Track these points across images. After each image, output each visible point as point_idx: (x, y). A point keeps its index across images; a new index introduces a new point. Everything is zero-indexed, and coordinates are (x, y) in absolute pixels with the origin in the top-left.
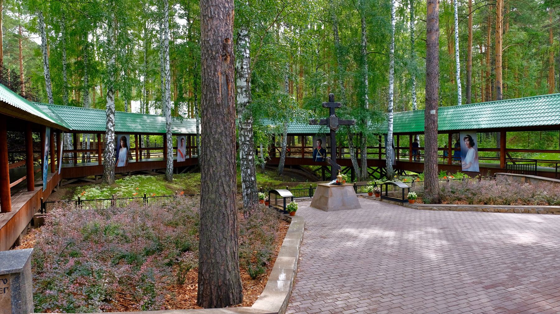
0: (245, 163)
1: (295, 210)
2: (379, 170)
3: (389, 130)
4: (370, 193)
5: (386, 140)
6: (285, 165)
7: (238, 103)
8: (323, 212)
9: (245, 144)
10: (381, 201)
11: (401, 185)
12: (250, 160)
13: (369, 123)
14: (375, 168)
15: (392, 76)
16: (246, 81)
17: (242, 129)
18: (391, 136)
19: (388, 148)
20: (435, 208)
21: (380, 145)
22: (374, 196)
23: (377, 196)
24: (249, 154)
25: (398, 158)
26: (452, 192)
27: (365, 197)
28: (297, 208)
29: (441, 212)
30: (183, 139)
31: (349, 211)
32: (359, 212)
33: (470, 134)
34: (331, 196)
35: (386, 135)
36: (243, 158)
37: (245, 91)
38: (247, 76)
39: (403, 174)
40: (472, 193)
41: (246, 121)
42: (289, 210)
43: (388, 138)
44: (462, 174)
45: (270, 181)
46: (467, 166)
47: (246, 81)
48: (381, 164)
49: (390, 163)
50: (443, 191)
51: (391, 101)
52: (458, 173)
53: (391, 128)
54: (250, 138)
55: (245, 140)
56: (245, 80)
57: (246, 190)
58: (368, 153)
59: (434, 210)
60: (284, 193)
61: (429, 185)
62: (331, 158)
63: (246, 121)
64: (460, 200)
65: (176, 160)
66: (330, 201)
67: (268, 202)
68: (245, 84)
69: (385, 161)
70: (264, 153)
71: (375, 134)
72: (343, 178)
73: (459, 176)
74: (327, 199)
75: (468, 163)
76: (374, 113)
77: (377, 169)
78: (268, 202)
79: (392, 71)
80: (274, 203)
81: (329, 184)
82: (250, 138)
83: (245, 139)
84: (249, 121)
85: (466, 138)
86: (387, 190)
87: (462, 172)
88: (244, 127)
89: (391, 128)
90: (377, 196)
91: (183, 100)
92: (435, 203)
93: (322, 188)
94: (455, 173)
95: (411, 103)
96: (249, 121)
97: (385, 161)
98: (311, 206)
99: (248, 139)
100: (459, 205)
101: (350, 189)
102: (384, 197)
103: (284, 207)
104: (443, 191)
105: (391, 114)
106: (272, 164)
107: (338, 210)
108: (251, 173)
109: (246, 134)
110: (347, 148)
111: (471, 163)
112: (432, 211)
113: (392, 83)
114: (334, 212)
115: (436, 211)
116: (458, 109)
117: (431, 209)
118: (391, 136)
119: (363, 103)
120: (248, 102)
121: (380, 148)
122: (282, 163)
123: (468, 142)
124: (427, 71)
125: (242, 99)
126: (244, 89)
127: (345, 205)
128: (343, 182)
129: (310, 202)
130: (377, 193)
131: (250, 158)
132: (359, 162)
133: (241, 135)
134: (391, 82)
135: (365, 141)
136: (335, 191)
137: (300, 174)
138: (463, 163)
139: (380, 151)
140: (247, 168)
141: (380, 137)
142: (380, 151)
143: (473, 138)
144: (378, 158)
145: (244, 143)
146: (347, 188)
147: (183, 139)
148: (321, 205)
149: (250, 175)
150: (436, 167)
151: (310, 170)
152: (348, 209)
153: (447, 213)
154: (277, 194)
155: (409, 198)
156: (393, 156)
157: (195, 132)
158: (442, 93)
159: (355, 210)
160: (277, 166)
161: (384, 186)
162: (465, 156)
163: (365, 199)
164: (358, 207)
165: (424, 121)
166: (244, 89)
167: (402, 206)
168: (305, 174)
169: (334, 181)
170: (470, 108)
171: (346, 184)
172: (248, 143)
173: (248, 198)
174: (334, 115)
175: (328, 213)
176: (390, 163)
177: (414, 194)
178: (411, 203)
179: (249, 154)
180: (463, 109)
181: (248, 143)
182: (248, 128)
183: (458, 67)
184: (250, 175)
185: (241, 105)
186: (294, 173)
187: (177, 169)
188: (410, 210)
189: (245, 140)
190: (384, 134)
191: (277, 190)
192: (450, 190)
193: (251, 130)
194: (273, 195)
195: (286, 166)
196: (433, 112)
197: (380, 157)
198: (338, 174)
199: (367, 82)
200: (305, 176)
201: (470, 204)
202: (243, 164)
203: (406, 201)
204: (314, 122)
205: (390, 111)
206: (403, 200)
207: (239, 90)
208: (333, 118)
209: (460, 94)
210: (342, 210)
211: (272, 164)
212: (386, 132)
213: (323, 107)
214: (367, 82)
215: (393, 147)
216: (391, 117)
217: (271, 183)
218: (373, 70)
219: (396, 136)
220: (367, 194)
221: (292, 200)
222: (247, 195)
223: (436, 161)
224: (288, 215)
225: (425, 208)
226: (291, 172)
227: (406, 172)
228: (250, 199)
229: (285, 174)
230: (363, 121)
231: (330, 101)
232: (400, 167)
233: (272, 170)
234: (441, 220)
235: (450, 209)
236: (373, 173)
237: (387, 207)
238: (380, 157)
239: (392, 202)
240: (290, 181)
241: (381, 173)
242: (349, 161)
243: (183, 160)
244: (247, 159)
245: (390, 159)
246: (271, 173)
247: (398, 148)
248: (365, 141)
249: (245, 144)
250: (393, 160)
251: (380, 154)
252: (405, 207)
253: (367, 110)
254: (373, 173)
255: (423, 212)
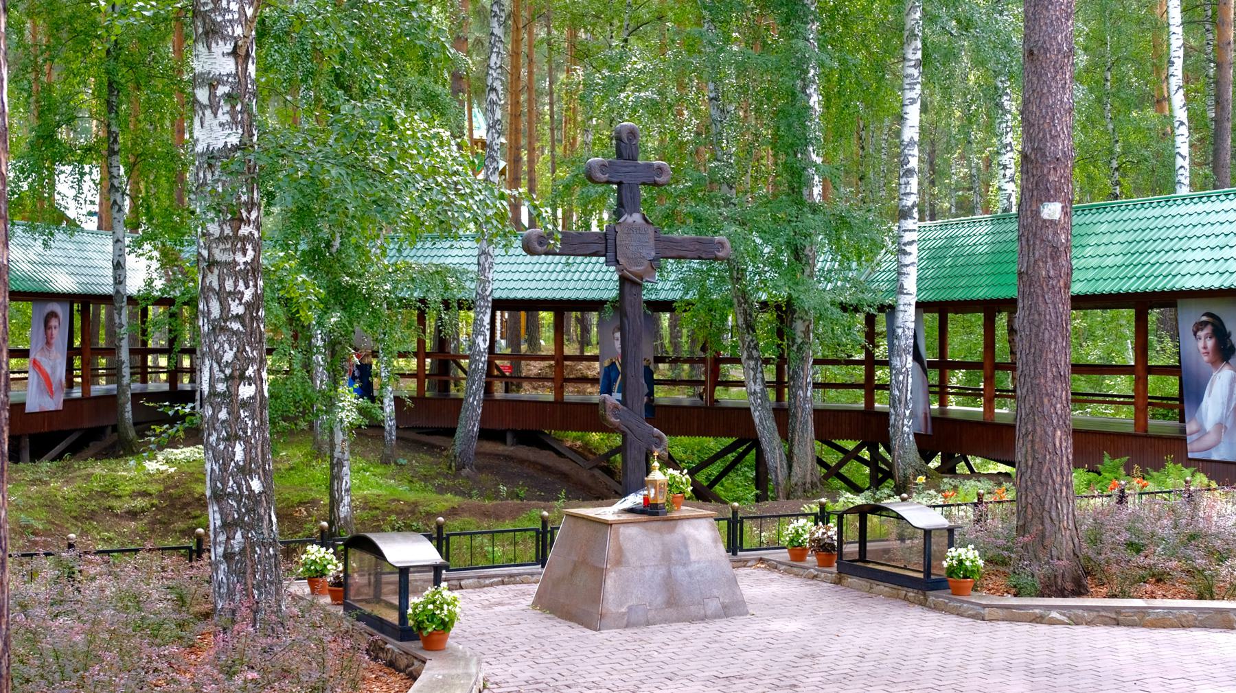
0: (223, 415)
1: (445, 625)
2: (865, 454)
3: (900, 290)
4: (797, 550)
5: (892, 334)
6: (481, 430)
7: (200, 148)
8: (578, 631)
9: (224, 329)
10: (838, 582)
11: (921, 513)
12: (244, 404)
13: (824, 261)
14: (850, 445)
15: (916, 72)
16: (234, 53)
17: (212, 264)
18: (907, 317)
19: (896, 362)
20: (1054, 614)
21: (870, 355)
22: (811, 559)
23: (825, 563)
24: (242, 377)
25: (943, 403)
26: (1130, 544)
27: (773, 566)
28: (452, 617)
29: (1080, 630)
30: (53, 315)
31: (690, 629)
32: (736, 630)
33: (1215, 311)
34: (618, 563)
35: (890, 310)
36: (213, 393)
37: (229, 97)
38: (239, 31)
39: (961, 468)
40: (1210, 553)
41: (228, 231)
42: (419, 624)
43: (899, 322)
44: (1187, 472)
45: (412, 497)
46: (1209, 440)
47: (234, 53)
48: (873, 427)
49: (906, 427)
50: (1095, 540)
51: (909, 172)
52: (1170, 465)
53: (910, 283)
54: (248, 306)
55: (225, 315)
56: (229, 47)
57: (222, 538)
58: (817, 385)
59: (1053, 622)
60: (408, 551)
61: (1033, 516)
62: (624, 402)
63: (228, 231)
64: (1159, 579)
65: (22, 405)
66: (611, 582)
67: (340, 588)
68: (228, 66)
69: (886, 415)
70: (399, 375)
71: (844, 308)
72: (672, 485)
73: (1175, 476)
74: (599, 574)
75: (1209, 425)
76: (843, 222)
77: (859, 448)
78: (340, 588)
79: (914, 53)
80: (368, 592)
81: (608, 512)
82: (248, 306)
83: (224, 307)
84: (245, 230)
85: (1200, 326)
86: (863, 540)
87: (1189, 462)
88: (219, 256)
89: (910, 283)
90: (825, 563)
91: (62, 154)
92: (1062, 594)
93: (583, 528)
94: (1159, 466)
95: (996, 184)
96: (245, 230)
97: (886, 415)
98: (534, 605)
99: (236, 309)
100: (1158, 602)
101: (701, 533)
102: (852, 564)
103: (403, 617)
104: (1095, 540)
105: (909, 224)
106: (426, 423)
107: (648, 623)
108: (249, 459)
109: (229, 285)
110: (735, 360)
111: (1220, 426)
112: (1043, 629)
113: (913, 101)
114: (629, 632)
115: (1060, 629)
116: (1174, 210)
117: (1039, 620)
118: (907, 317)
119: (797, 178)
120: (242, 147)
121: (871, 363)
122: (470, 422)
123: (1210, 343)
124: (1027, 38)
125: (213, 132)
126: (222, 90)
127: (677, 603)
128: (673, 502)
129: (535, 588)
130: (825, 549)
131: (246, 391)
132: (783, 416)
133: (206, 291)
134: (910, 94)
135: (807, 332)
136: (637, 540)
137: (546, 469)
138: (1190, 427)
139: (870, 375)
140: (231, 438)
141: (870, 320)
142: (870, 375)
143: (1229, 327)
144: (861, 405)
145: (218, 328)
146: (688, 529)
147: (53, 315)
148: (575, 603)
149: (245, 471)
150: (1063, 443)
151: (586, 451)
152: (692, 619)
153: (1102, 635)
154: (379, 554)
155: (951, 571)
156: (921, 397)
157: (110, 290)
158: (1118, 149)
159: (720, 624)
160: (450, 432)
161: (852, 521)
162: (1199, 399)
163: (775, 575)
164: (733, 608)
165: (1016, 246)
166: (222, 90)
167: (923, 604)
168: (563, 465)
169: (634, 500)
170: (1218, 206)
171: (686, 510)
172: (236, 326)
173: (229, 572)
174: (637, 217)
175: (606, 634)
176: (906, 427)
177: (970, 555)
178: (957, 592)
179: (242, 377)
180: (1191, 208)
181: (236, 326)
182: (240, 259)
183: (1177, 42)
184: (245, 471)
185: (211, 158)
186: (522, 461)
187: (26, 443)
188: (951, 621)
189: (225, 315)
190: (882, 308)
191: (374, 537)
192: (1125, 536)
193: (253, 270)
194: (357, 559)
195: (485, 434)
196: (1052, 210)
197: (870, 400)
198: (648, 471)
199: (815, 100)
200: (564, 477)
201: (1201, 597)
202: (214, 416)
203: (939, 585)
204: (577, 244)
205: (904, 214)
206: (926, 581)
207: (202, 95)
208: (631, 228)
209: (1184, 149)
210: (667, 621)
211: (426, 423)
212: (888, 301)
213: (591, 178)
214: (815, 100)
215: (917, 357)
216: (908, 237)
217: (416, 504)
218: (837, 42)
219: (932, 318)
220: (784, 555)
221: (437, 582)
222: (228, 556)
223: (1064, 418)
224: (414, 647)
225: (1013, 616)
226: (508, 458)
227: (976, 461)
228: (241, 574)
229: (480, 469)
230: (797, 253)
231: (619, 155)
232: (948, 442)
233: (431, 448)
234: (1073, 669)
235: (1117, 619)
236: (841, 464)
237: (860, 612)
238: (870, 400)
239: (883, 588)
240: (497, 495)
241: (873, 464)
242: (742, 414)
243: (53, 403)
244: (229, 396)
245: (907, 402)
246: (420, 462)
247: (944, 365)
248: (807, 332)
249: (224, 329)
250: (921, 414)
251: (870, 387)
252: (936, 608)
253: (814, 209)
254: (841, 464)
255: (1004, 629)
